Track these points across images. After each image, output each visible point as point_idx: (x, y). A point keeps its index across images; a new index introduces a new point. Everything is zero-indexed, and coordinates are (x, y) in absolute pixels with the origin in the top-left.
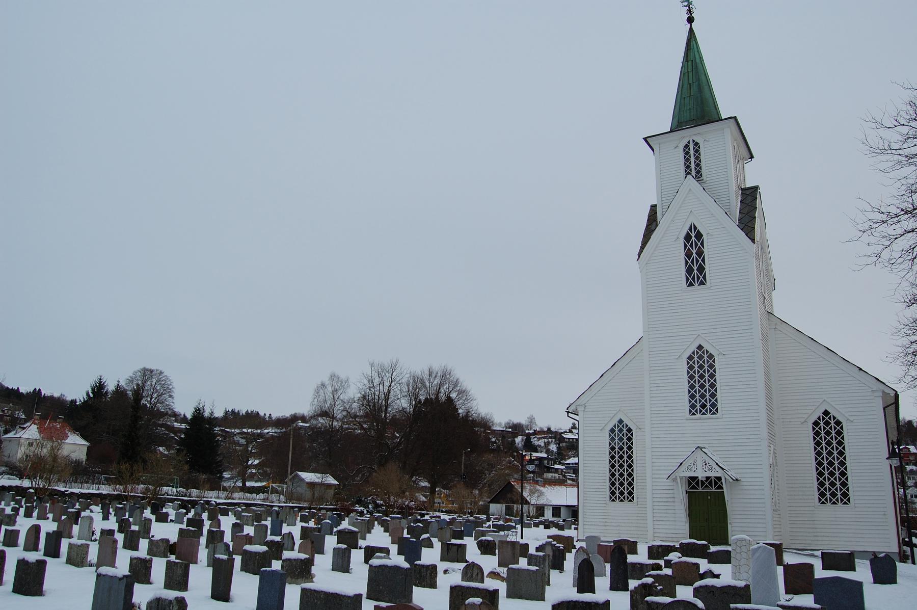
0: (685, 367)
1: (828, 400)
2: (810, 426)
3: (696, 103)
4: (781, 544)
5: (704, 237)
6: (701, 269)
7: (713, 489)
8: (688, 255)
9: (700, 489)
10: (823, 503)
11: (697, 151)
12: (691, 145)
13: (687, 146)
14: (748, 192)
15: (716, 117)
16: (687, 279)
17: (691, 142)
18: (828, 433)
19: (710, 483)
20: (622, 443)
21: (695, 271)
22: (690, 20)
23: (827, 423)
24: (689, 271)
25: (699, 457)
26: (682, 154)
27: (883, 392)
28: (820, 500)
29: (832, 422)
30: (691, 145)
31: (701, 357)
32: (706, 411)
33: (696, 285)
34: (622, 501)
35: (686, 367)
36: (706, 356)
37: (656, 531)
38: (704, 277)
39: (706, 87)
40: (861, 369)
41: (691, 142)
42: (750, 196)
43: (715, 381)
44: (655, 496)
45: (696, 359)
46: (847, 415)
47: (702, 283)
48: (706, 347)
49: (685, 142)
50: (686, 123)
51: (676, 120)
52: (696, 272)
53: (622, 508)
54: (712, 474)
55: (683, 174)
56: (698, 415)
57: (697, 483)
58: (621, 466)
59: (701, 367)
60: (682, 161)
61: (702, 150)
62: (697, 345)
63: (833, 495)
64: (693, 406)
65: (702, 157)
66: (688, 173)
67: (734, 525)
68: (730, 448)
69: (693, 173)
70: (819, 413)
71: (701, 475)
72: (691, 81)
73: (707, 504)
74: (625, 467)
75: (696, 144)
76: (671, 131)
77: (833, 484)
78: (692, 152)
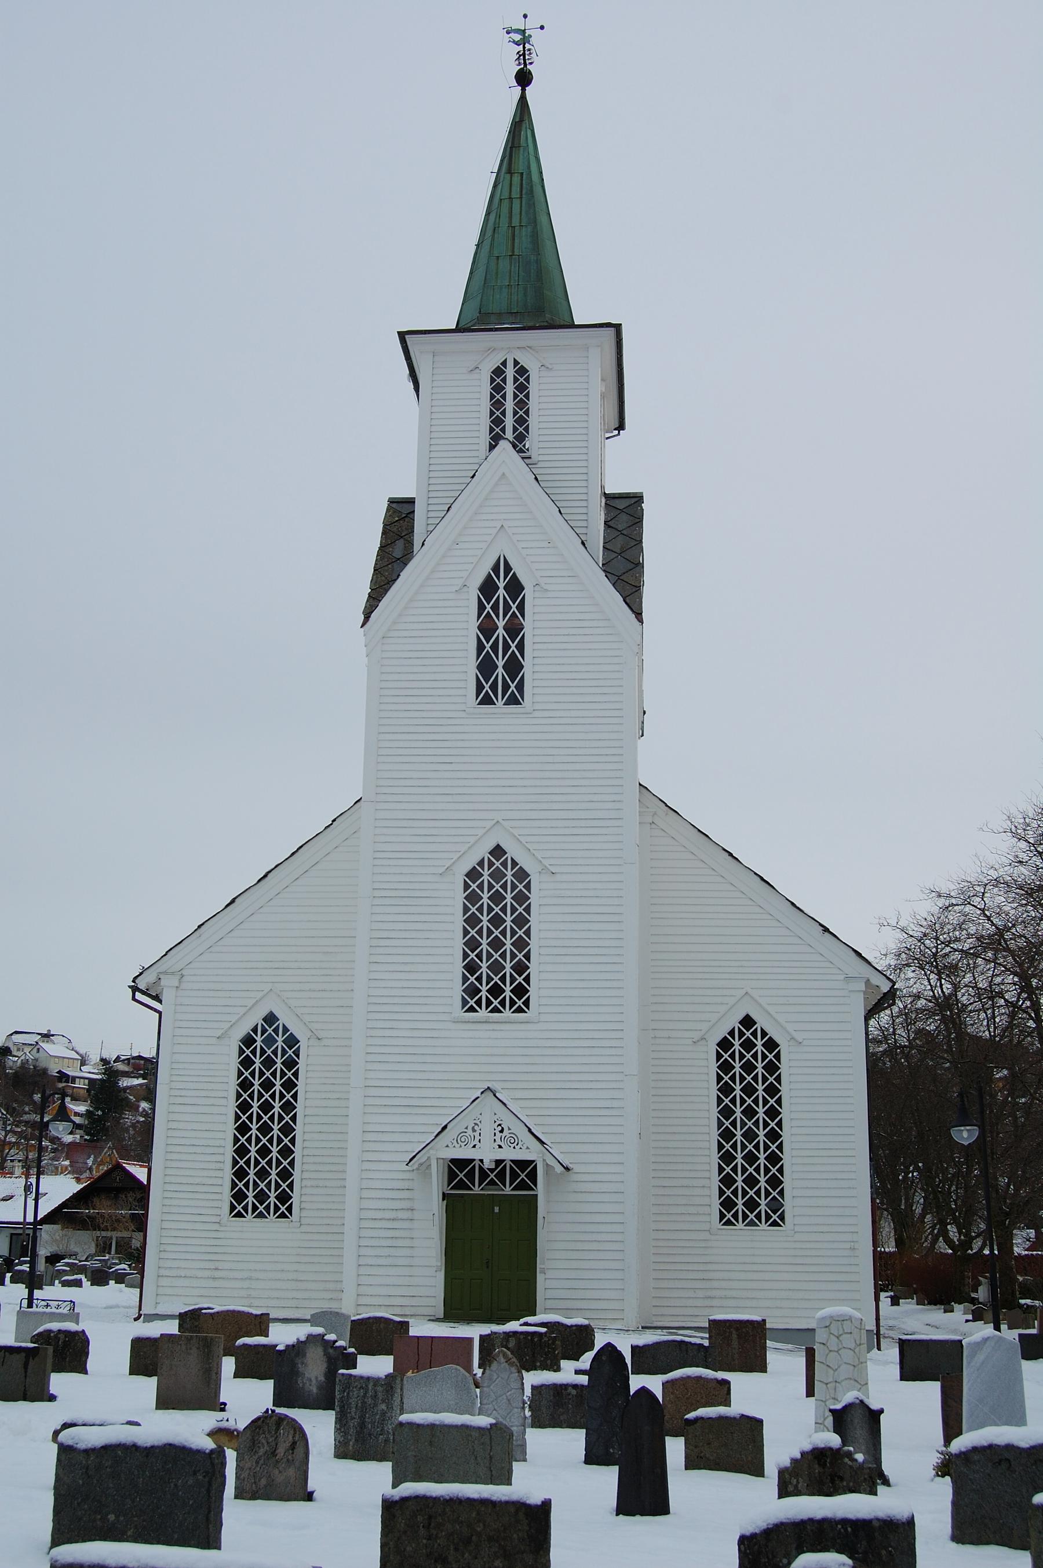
0: (459, 897)
1: (754, 994)
2: (713, 1048)
3: (517, 278)
4: (764, 1321)
5: (528, 592)
6: (514, 667)
7: (508, 1190)
8: (487, 629)
9: (477, 1190)
10: (729, 1223)
11: (521, 389)
12: (510, 372)
13: (498, 372)
14: (621, 504)
15: (568, 322)
16: (480, 687)
17: (510, 364)
18: (748, 1064)
19: (501, 1175)
20: (268, 1070)
21: (500, 670)
22: (524, 78)
23: (748, 1045)
24: (486, 667)
25: (488, 1112)
26: (486, 389)
27: (868, 982)
28: (722, 1216)
29: (759, 1043)
30: (510, 372)
31: (497, 875)
32: (503, 1003)
33: (500, 703)
34: (261, 1215)
35: (460, 896)
36: (509, 873)
37: (363, 1290)
38: (520, 687)
39: (548, 243)
40: (826, 930)
41: (510, 364)
42: (625, 514)
43: (528, 933)
44: (366, 1204)
45: (486, 877)
46: (790, 1028)
47: (513, 701)
48: (513, 851)
49: (496, 363)
50: (500, 316)
51: (475, 304)
52: (500, 673)
53: (261, 1233)
54: (509, 1154)
55: (485, 438)
56: (483, 1013)
57: (470, 1175)
58: (265, 1129)
59: (497, 898)
60: (485, 405)
61: (533, 388)
62: (491, 846)
63: (752, 1205)
64: (472, 991)
65: (533, 404)
66: (495, 439)
67: (550, 1274)
68: (552, 1094)
69: (509, 434)
70: (733, 1021)
71: (487, 1154)
72: (515, 222)
73: (491, 1220)
74: (276, 1132)
75: (522, 371)
76: (459, 329)
77: (751, 1184)
78: (510, 388)
